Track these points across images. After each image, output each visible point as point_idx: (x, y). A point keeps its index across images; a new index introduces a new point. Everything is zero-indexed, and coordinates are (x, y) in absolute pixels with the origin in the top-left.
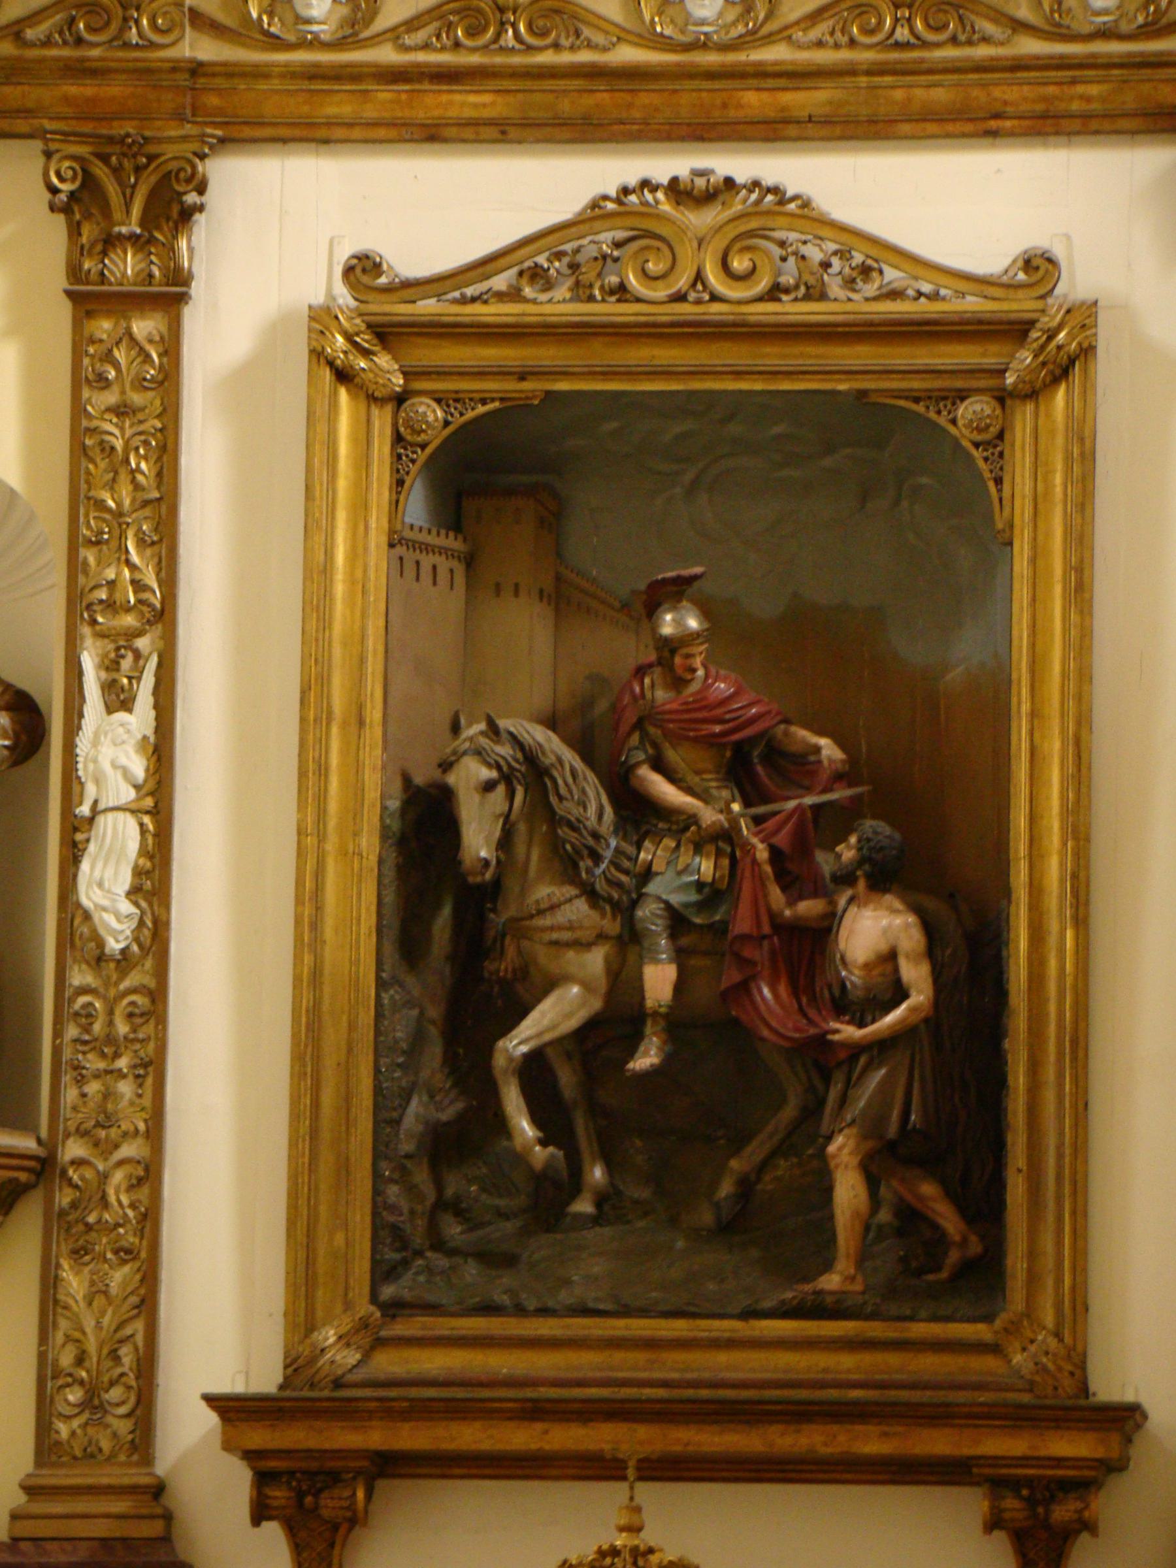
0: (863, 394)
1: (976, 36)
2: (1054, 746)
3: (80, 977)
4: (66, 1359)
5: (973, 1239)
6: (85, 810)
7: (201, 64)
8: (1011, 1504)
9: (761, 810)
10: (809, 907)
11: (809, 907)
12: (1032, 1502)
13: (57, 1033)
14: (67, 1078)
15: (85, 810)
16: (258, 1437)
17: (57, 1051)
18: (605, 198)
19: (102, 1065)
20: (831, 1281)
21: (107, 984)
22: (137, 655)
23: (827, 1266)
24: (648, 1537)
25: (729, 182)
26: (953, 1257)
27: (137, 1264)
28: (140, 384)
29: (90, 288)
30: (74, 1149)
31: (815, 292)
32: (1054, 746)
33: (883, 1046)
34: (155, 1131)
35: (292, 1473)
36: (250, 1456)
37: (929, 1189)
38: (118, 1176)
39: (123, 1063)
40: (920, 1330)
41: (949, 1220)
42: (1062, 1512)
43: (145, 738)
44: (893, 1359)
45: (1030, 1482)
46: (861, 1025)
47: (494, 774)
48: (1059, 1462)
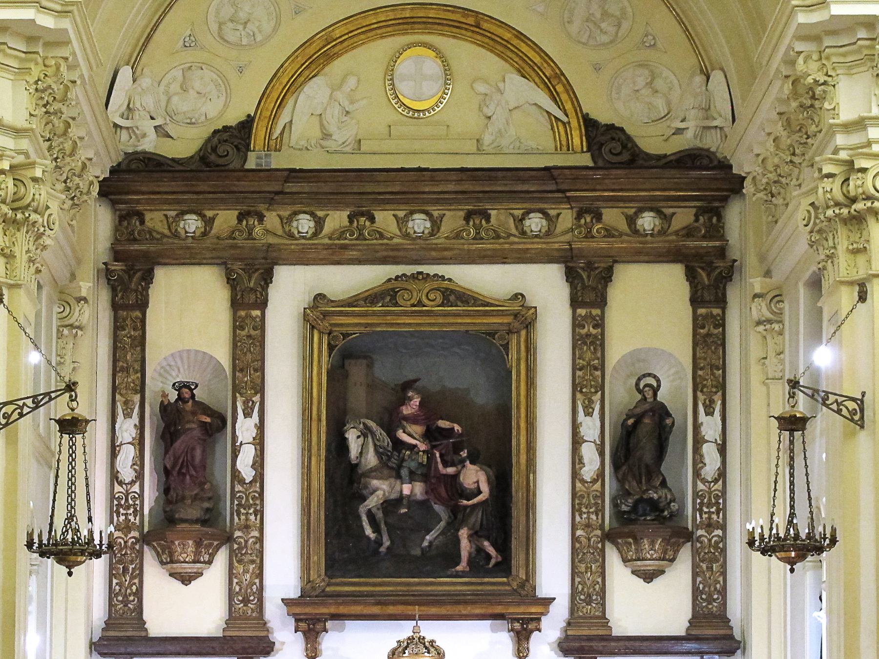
0: (467, 331)
1: (361, 237)
2: (523, 425)
3: (238, 488)
4: (237, 588)
5: (499, 556)
6: (238, 444)
7: (271, 244)
8: (517, 626)
9: (434, 443)
10: (451, 470)
11: (451, 470)
12: (522, 624)
13: (232, 503)
14: (577, 514)
15: (238, 444)
16: (298, 610)
17: (232, 508)
18: (391, 278)
19: (125, 512)
20: (459, 568)
21: (246, 490)
22: (253, 402)
23: (458, 564)
24: (422, 634)
25: (428, 275)
26: (493, 562)
27: (598, 564)
28: (255, 328)
29: (44, 310)
30: (238, 534)
31: (454, 305)
32: (523, 425)
33: (474, 506)
34: (261, 530)
35: (307, 619)
36: (294, 615)
37: (486, 544)
38: (251, 540)
39: (251, 511)
40: (486, 580)
41: (491, 551)
42: (319, 627)
43: (256, 424)
44: (480, 588)
45: (522, 619)
46: (468, 500)
47: (360, 434)
48: (531, 613)
